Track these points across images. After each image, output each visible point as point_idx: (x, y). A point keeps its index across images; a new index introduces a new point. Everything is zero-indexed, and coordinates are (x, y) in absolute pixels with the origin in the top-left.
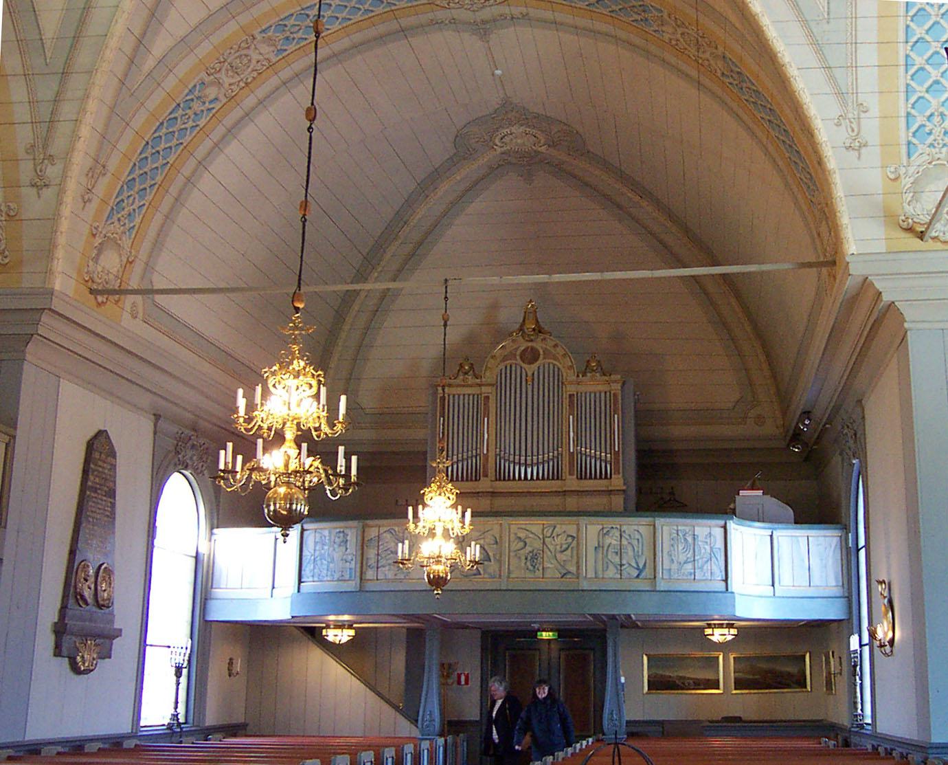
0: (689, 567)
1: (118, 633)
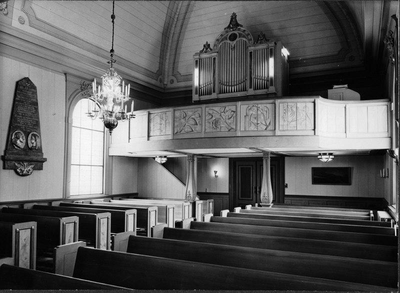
0: (294, 123)
1: (45, 160)
